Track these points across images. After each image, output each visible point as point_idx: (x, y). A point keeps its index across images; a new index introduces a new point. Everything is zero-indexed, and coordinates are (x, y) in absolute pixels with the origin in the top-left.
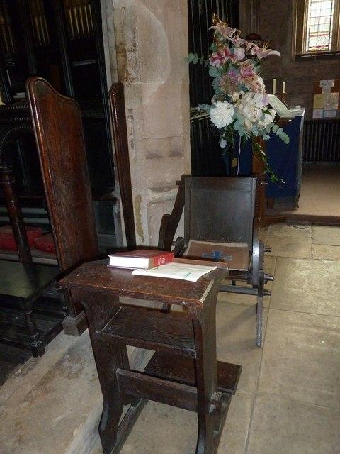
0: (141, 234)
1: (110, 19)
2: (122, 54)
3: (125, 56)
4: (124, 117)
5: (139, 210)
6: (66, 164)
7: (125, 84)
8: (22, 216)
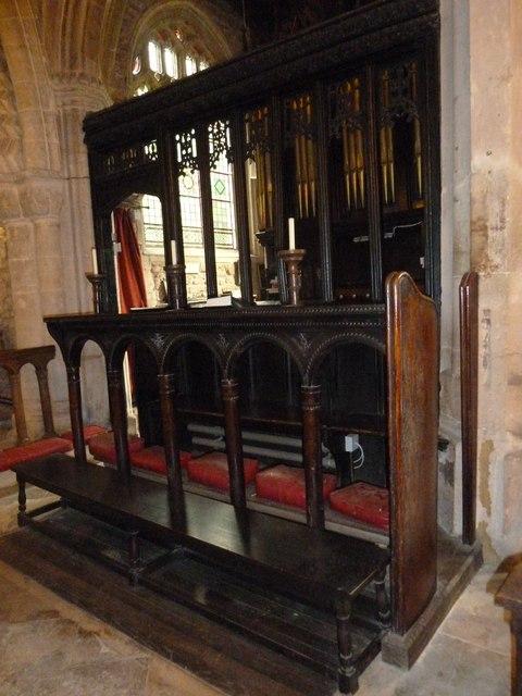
0: (487, 503)
1: (460, 187)
2: (481, 233)
3: (486, 236)
4: (475, 320)
5: (486, 464)
6: (419, 391)
7: (481, 274)
8: (242, 442)
